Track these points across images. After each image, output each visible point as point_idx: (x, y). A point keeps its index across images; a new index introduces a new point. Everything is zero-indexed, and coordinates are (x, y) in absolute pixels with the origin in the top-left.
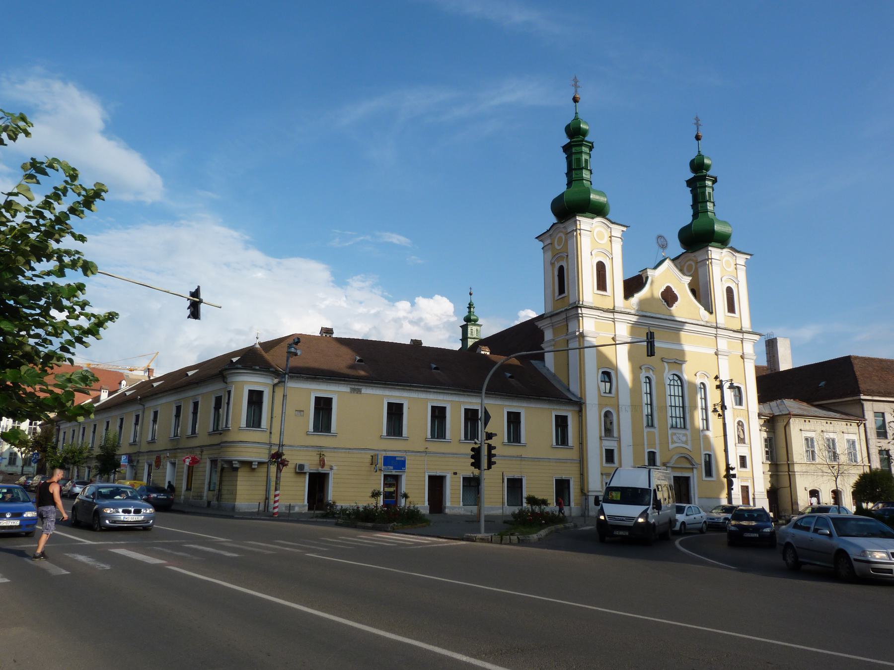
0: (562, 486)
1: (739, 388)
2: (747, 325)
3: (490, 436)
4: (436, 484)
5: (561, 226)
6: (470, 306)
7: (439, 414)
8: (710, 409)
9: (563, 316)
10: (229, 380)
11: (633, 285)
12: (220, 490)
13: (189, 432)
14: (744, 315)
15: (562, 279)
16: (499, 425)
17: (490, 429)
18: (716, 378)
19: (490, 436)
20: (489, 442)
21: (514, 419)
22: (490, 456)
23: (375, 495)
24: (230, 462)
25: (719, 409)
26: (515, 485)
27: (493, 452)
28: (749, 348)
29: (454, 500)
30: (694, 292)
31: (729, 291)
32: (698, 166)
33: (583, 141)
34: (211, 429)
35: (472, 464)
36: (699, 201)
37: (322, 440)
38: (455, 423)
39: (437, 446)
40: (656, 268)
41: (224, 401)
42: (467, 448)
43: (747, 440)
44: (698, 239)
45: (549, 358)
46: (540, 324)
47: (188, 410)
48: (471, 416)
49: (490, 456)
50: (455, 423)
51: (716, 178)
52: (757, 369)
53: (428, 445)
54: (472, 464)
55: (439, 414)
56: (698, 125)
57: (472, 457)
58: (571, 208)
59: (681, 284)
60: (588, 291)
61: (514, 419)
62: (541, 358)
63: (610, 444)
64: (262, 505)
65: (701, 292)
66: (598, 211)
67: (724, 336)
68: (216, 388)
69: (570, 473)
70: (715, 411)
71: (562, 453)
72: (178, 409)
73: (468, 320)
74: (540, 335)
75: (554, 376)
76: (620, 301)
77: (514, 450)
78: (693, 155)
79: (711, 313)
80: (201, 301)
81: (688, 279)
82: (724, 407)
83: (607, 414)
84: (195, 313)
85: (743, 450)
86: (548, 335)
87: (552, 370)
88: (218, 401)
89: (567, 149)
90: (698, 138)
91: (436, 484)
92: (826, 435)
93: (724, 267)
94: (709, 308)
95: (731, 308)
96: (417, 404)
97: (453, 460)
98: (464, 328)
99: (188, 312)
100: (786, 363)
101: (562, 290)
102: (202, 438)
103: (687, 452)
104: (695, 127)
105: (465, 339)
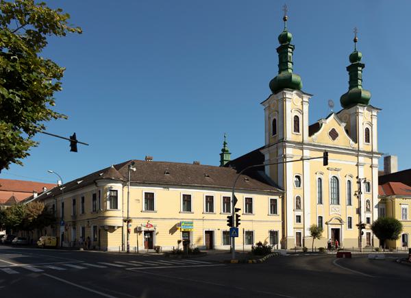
0: (273, 234)
1: (369, 183)
2: (375, 149)
3: (237, 210)
4: (210, 234)
5: (275, 96)
6: (225, 144)
7: (210, 200)
8: (353, 193)
9: (275, 146)
10: (99, 184)
11: (314, 129)
12: (99, 240)
13: (81, 212)
14: (374, 145)
15: (275, 128)
16: (241, 204)
17: (236, 207)
18: (357, 177)
19: (237, 210)
20: (237, 213)
21: (249, 202)
22: (238, 220)
23: (179, 242)
24: (103, 227)
25: (357, 193)
26: (250, 235)
27: (239, 218)
28: (375, 161)
29: (219, 244)
30: (347, 131)
31: (367, 130)
32: (354, 58)
33: (289, 44)
34: (92, 211)
35: (228, 225)
36: (354, 80)
37: (150, 214)
38: (218, 204)
39: (209, 216)
40: (326, 119)
41: (97, 196)
42: (225, 217)
43: (302, 208)
44: (352, 100)
45: (267, 168)
46: (262, 151)
47: (79, 201)
48: (226, 201)
49: (238, 220)
50: (218, 204)
51: (364, 65)
52: (379, 172)
53: (204, 215)
54: (228, 225)
55: (210, 200)
56: (355, 32)
57: (228, 221)
58: (281, 85)
59: (341, 129)
60: (290, 134)
61: (249, 202)
62: (263, 168)
63: (299, 213)
64: (121, 248)
65: (352, 132)
66: (295, 86)
67: (361, 156)
68: (93, 189)
69: (301, 231)
70: (355, 194)
71: (274, 218)
72: (74, 201)
73: (224, 150)
74: (263, 157)
75: (268, 178)
76: (307, 139)
77: (249, 217)
78: (352, 52)
79: (356, 143)
80: (77, 142)
81: (344, 124)
82: (360, 192)
83: (298, 198)
84: (74, 149)
85: (369, 215)
86: (267, 157)
87: (269, 176)
88: (94, 196)
89: (279, 50)
90: (355, 41)
91: (210, 234)
92: (403, 206)
93: (365, 117)
94: (356, 140)
95: (367, 140)
96: (199, 196)
97: (219, 224)
98: (222, 155)
99: (70, 148)
100: (394, 170)
101: (274, 132)
102: (88, 215)
103: (337, 216)
104: (354, 34)
105: (222, 161)
